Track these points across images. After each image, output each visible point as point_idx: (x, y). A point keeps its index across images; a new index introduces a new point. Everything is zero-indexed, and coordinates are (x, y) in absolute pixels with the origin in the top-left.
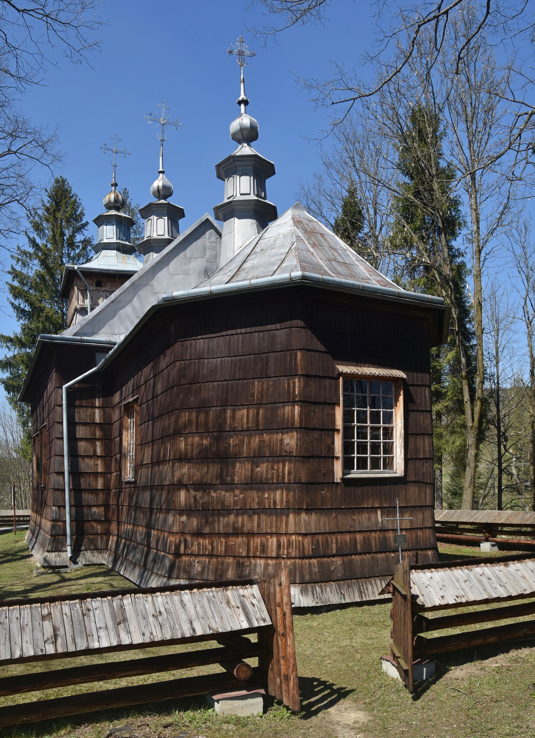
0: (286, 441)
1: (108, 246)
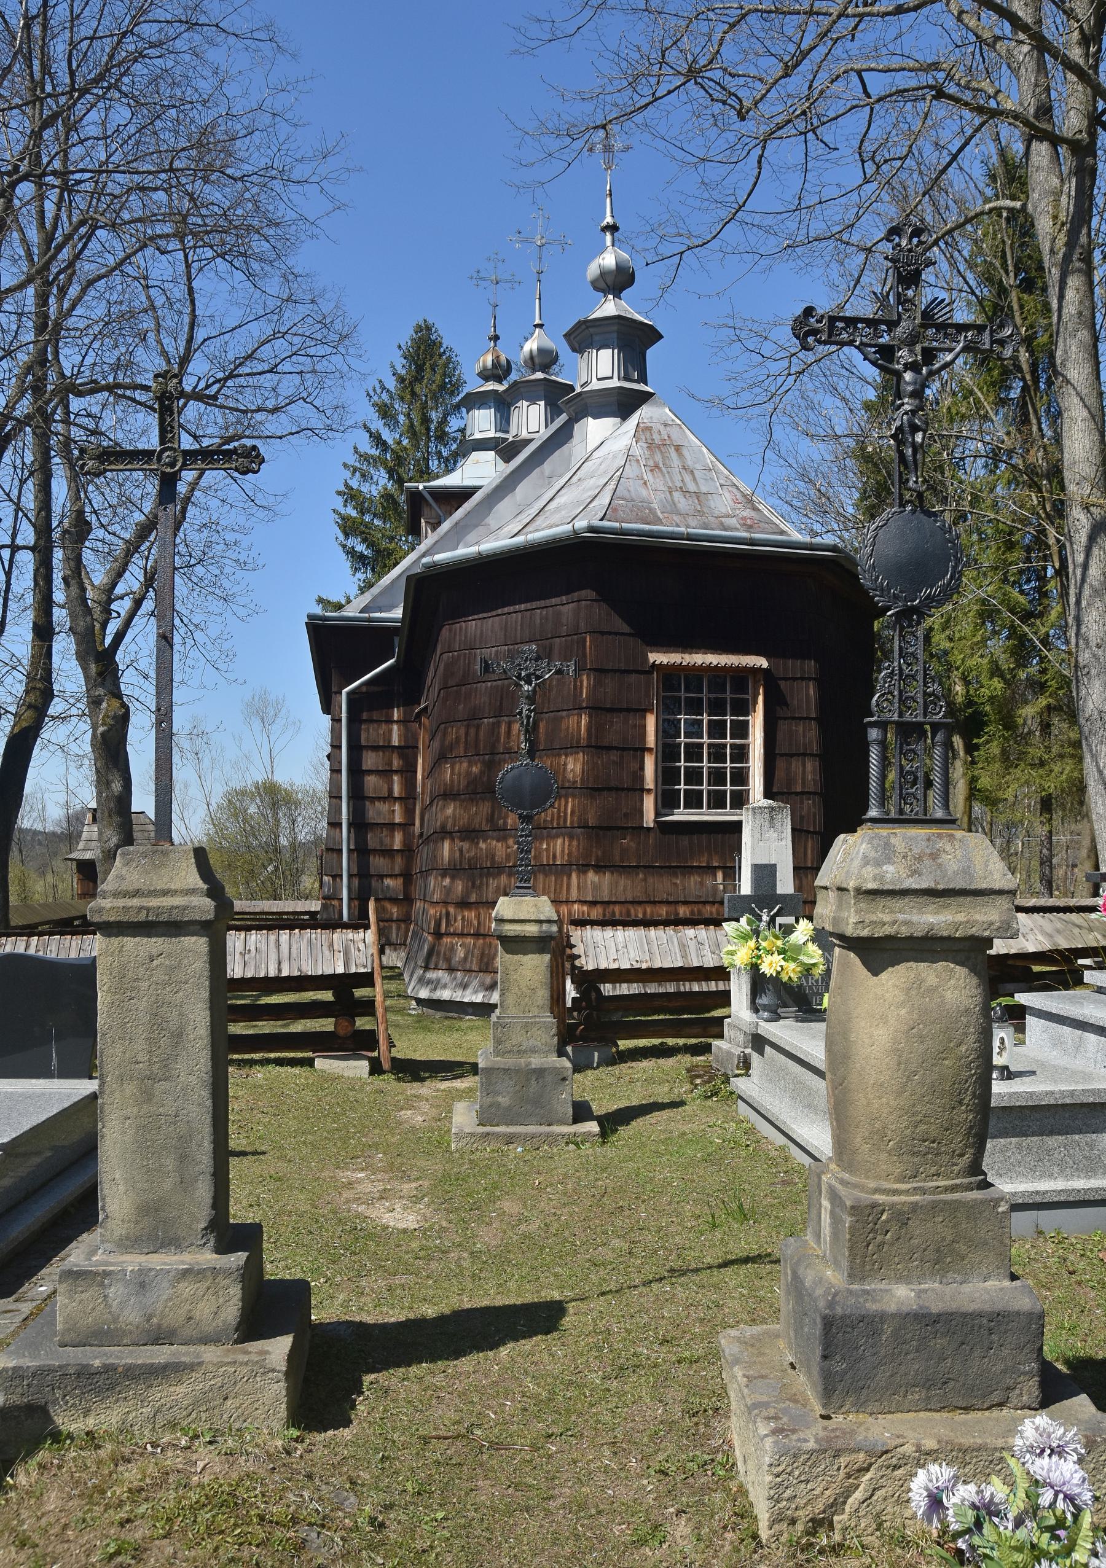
0: (570, 766)
1: (482, 445)
